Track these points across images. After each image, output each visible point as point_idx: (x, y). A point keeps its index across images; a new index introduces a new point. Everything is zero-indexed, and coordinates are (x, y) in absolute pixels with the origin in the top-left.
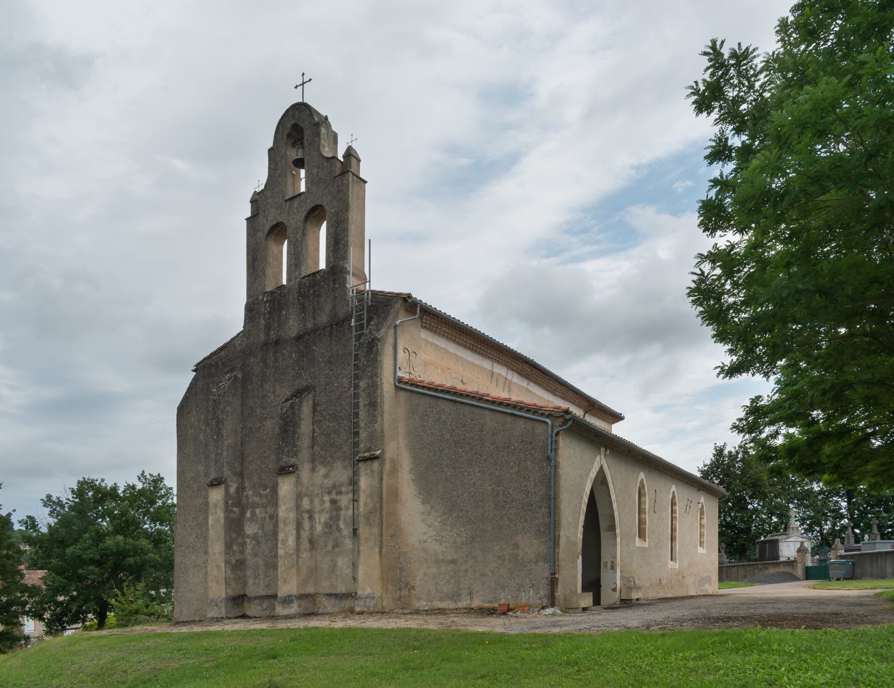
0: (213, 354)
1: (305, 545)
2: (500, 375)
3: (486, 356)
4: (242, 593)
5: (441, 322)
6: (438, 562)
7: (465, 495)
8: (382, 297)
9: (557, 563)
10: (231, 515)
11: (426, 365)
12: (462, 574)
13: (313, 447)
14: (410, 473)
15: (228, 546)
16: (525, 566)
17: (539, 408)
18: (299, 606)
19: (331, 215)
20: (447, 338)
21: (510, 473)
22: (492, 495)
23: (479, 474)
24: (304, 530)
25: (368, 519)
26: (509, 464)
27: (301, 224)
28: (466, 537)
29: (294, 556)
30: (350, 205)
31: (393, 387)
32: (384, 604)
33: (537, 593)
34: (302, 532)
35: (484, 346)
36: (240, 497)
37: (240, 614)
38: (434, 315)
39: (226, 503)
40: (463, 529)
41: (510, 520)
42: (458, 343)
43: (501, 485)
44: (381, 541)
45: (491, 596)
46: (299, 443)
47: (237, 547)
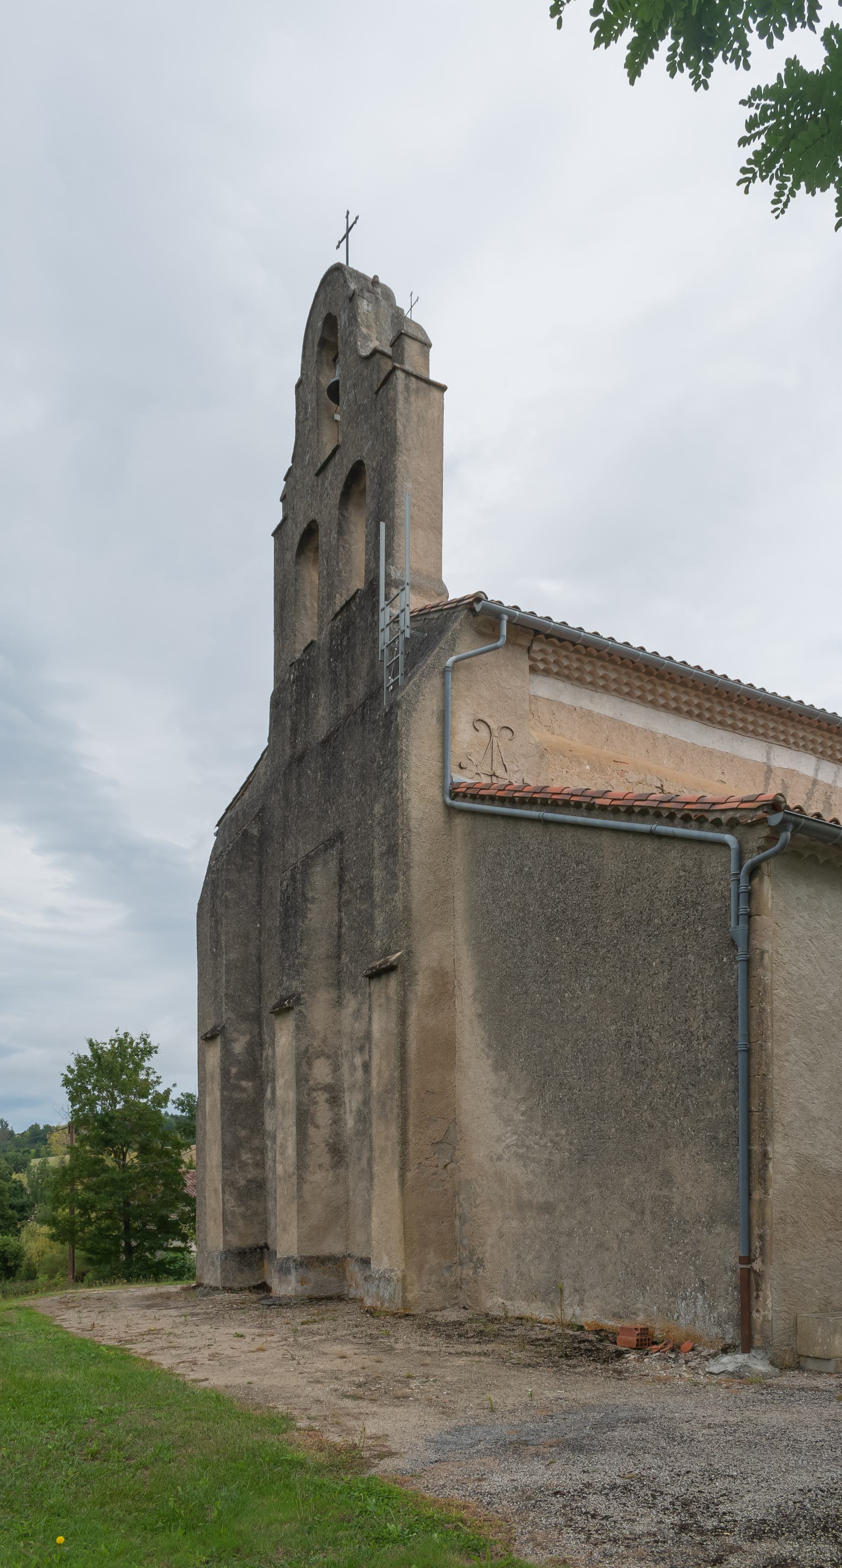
0: (237, 798)
1: (320, 1154)
2: (792, 773)
3: (744, 730)
4: (262, 1243)
5: (588, 654)
6: (522, 1206)
7: (568, 1048)
8: (436, 616)
9: (756, 1231)
10: (236, 1095)
11: (542, 756)
12: (563, 1240)
13: (339, 957)
14: (474, 1000)
15: (230, 1154)
16: (684, 1231)
17: (707, 807)
18: (302, 1282)
19: (372, 473)
20: (618, 692)
21: (653, 989)
22: (617, 1045)
23: (592, 996)
24: (317, 1127)
25: (383, 1106)
26: (650, 964)
27: (335, 512)
28: (569, 1151)
29: (294, 1179)
30: (401, 439)
31: (440, 809)
32: (410, 1296)
33: (712, 1308)
34: (312, 1131)
35: (731, 707)
36: (255, 1060)
37: (253, 1283)
38: (561, 640)
39: (225, 1073)
40: (563, 1132)
41: (653, 1110)
42: (654, 704)
43: (635, 1020)
44: (404, 1155)
45: (618, 1301)
46: (304, 949)
47: (249, 1156)
